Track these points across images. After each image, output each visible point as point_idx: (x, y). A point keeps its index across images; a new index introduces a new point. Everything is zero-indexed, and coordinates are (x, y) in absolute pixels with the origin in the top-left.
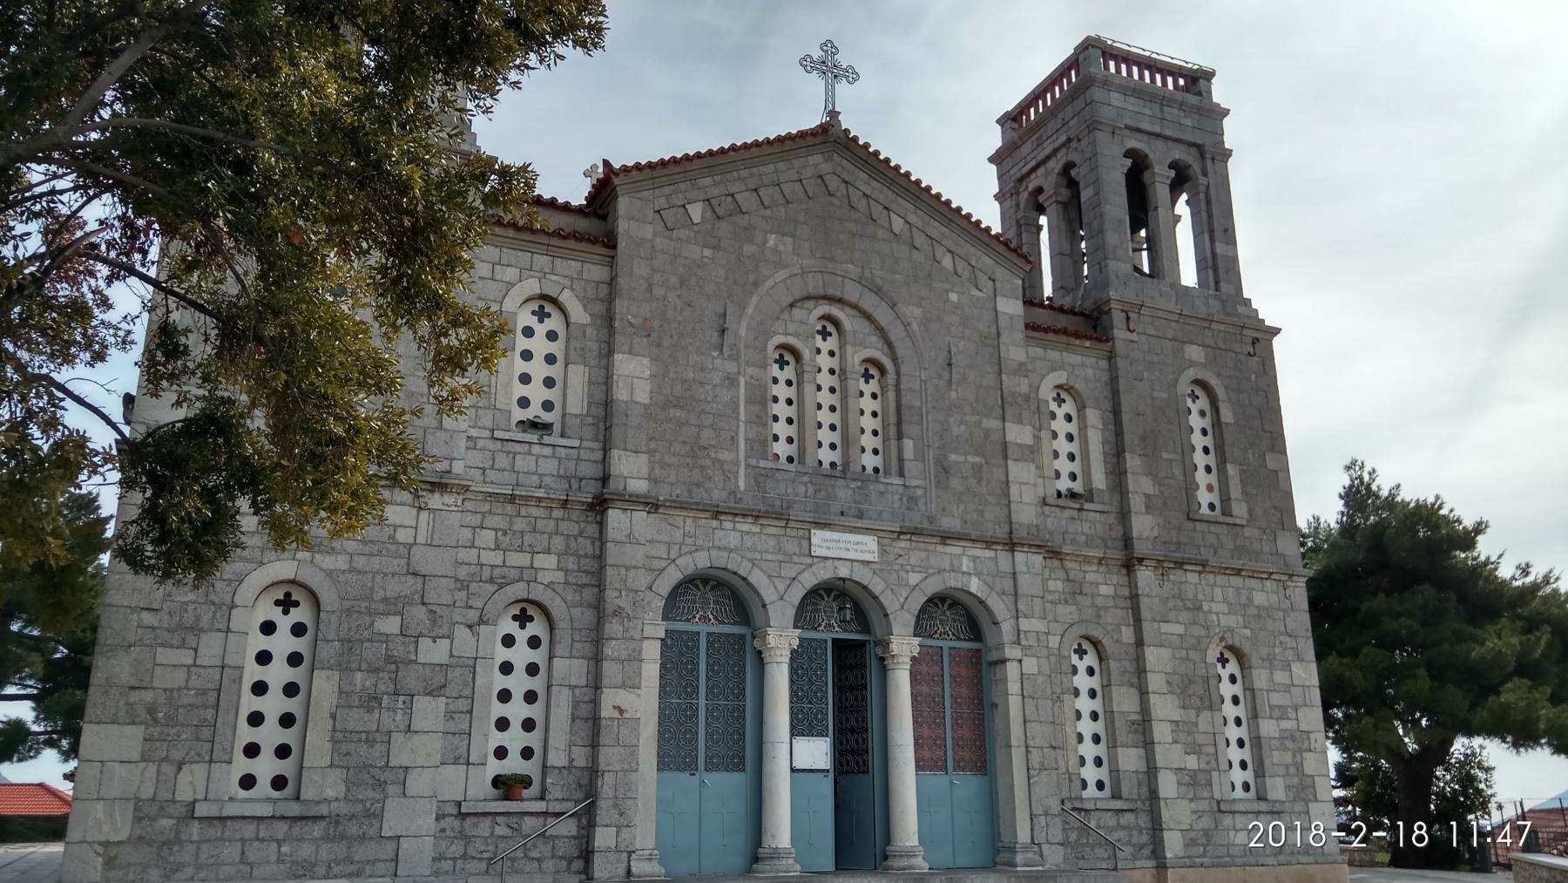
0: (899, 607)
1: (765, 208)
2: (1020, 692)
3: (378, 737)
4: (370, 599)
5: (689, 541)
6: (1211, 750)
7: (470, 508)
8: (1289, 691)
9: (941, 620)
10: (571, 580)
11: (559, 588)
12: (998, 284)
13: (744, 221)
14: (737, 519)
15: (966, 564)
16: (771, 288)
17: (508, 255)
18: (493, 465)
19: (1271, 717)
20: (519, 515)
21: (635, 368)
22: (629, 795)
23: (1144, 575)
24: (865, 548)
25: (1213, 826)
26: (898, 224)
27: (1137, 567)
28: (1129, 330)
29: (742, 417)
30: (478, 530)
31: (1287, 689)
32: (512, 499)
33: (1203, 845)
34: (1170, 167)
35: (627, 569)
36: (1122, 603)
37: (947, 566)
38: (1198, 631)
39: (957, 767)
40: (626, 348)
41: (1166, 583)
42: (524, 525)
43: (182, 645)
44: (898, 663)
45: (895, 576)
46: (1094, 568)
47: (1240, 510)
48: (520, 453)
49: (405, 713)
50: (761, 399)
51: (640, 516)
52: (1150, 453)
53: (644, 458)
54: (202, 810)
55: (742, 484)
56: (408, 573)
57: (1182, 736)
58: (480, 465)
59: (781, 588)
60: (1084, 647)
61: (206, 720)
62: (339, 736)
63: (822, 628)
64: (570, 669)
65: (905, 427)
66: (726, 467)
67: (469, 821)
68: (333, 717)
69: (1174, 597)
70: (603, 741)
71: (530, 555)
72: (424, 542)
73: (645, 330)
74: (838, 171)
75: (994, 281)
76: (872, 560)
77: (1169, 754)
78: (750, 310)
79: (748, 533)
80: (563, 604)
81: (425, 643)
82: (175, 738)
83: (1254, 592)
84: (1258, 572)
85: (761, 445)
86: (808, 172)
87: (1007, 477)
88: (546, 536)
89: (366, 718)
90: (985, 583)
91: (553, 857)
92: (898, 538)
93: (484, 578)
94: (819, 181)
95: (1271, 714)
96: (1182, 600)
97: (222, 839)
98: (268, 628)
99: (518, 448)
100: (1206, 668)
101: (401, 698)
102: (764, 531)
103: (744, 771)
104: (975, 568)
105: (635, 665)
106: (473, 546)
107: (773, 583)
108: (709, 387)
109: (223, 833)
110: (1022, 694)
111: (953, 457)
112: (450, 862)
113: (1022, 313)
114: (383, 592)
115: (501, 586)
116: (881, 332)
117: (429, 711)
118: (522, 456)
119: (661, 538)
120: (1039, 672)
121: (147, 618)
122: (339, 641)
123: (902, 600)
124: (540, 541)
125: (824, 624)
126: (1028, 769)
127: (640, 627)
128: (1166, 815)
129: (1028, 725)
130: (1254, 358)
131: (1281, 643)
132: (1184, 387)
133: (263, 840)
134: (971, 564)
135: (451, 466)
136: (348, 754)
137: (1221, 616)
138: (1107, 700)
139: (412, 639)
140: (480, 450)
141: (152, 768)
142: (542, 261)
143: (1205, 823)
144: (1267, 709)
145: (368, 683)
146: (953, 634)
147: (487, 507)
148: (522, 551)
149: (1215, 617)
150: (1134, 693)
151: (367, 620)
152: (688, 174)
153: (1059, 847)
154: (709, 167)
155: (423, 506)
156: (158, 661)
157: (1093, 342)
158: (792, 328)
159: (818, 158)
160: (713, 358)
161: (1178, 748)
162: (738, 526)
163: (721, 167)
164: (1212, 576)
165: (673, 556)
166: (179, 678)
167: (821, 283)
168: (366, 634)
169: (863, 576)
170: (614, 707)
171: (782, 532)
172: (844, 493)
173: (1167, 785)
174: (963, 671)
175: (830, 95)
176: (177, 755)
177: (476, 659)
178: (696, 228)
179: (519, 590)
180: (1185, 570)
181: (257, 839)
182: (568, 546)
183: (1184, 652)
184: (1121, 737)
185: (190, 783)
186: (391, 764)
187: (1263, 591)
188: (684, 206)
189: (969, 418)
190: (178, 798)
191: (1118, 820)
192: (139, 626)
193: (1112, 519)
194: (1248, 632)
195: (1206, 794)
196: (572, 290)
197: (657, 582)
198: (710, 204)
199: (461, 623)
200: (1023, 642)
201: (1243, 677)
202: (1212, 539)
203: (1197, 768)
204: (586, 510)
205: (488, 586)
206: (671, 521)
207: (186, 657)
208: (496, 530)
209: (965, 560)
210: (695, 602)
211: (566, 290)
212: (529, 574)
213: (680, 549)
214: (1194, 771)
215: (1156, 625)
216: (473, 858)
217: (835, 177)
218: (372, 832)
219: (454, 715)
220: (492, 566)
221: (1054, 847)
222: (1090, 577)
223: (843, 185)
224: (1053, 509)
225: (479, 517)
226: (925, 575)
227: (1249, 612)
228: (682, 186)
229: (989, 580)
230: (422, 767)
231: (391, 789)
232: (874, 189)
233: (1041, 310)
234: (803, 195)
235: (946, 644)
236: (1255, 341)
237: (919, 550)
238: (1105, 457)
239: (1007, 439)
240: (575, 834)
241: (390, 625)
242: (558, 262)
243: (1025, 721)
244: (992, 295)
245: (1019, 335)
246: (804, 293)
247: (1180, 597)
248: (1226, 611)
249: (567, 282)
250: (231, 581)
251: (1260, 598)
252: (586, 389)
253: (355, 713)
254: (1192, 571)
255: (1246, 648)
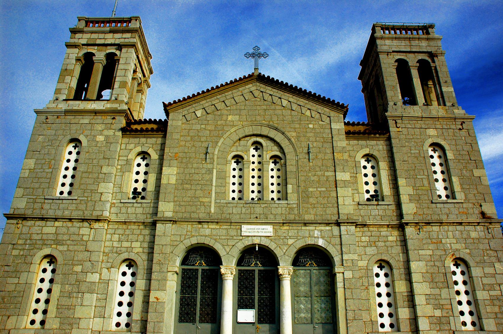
0: (283, 254)
1: (227, 107)
2: (343, 287)
4: (73, 260)
7: (111, 227)
8: (495, 277)
11: (140, 254)
14: (209, 224)
15: (316, 233)
17: (132, 140)
18: (120, 212)
19: (484, 290)
20: (128, 229)
21: (170, 171)
22: (159, 331)
24: (267, 231)
26: (285, 103)
29: (214, 184)
30: (113, 235)
32: (125, 223)
35: (163, 245)
37: (307, 235)
38: (439, 253)
40: (168, 165)
41: (421, 232)
42: (129, 232)
44: (283, 278)
46: (385, 229)
47: (460, 196)
48: (129, 207)
49: (81, 299)
50: (223, 177)
51: (169, 225)
52: (412, 177)
53: (172, 204)
55: (213, 210)
56: (86, 251)
57: (432, 301)
58: (116, 212)
59: (228, 250)
61: (19, 301)
62: (59, 306)
64: (141, 284)
65: (288, 180)
66: (206, 204)
68: (58, 300)
69: (426, 238)
70: (150, 310)
71: (130, 243)
72: (92, 240)
73: (176, 157)
74: (259, 88)
75: (330, 117)
76: (270, 235)
78: (219, 144)
79: (214, 229)
80: (141, 260)
82: (9, 307)
83: (470, 232)
84: (471, 223)
85: (221, 194)
86: (246, 91)
87: (337, 195)
88: (137, 235)
89: (68, 301)
90: (326, 240)
93: (114, 252)
94: (251, 93)
95: (484, 288)
96: (431, 239)
99: (129, 205)
101: (80, 294)
102: (221, 228)
104: (321, 235)
105: (164, 282)
106: (111, 240)
107: (224, 248)
110: (344, 287)
111: (311, 189)
114: (77, 257)
115: (119, 254)
117: (91, 299)
118: (130, 208)
119: (178, 233)
120: (353, 276)
121: (7, 268)
122: (62, 274)
123: (284, 251)
124: (135, 237)
126: (347, 320)
127: (166, 268)
129: (347, 300)
131: (487, 254)
135: (102, 213)
136: (61, 313)
137: (452, 245)
139: (85, 273)
140: (116, 207)
144: (481, 286)
145: (70, 289)
147: (117, 226)
148: (128, 241)
149: (449, 245)
152: (195, 101)
154: (204, 97)
155: (92, 227)
156: (7, 282)
158: (240, 148)
160: (203, 164)
161: (430, 307)
162: (210, 226)
163: (209, 96)
164: (446, 227)
167: (251, 130)
168: (71, 272)
169: (265, 242)
170: (155, 298)
171: (229, 227)
172: (258, 209)
176: (8, 313)
177: (109, 280)
178: (199, 119)
179: (125, 256)
180: (431, 226)
182: (144, 238)
183: (433, 262)
184: (399, 304)
186: (75, 317)
187: (475, 231)
188: (194, 112)
189: (319, 173)
192: (4, 271)
194: (468, 251)
195: (446, 328)
196: (153, 148)
197: (175, 250)
198: (205, 110)
199: (105, 268)
203: (441, 316)
204: (152, 225)
205: (115, 254)
207: (16, 281)
208: (119, 234)
209: (316, 232)
211: (150, 148)
212: (130, 249)
213: (185, 237)
214: (440, 317)
215: (416, 252)
217: (257, 91)
219: (100, 300)
220: (117, 247)
222: (383, 234)
223: (261, 93)
225: (114, 230)
228: (194, 105)
230: (85, 318)
231: (74, 326)
232: (274, 92)
234: (244, 100)
238: (389, 181)
242: (149, 139)
243: (345, 299)
244: (329, 122)
246: (244, 135)
248: (455, 242)
249: (151, 146)
250: (32, 255)
251: (473, 235)
253: (65, 299)
255: (467, 258)
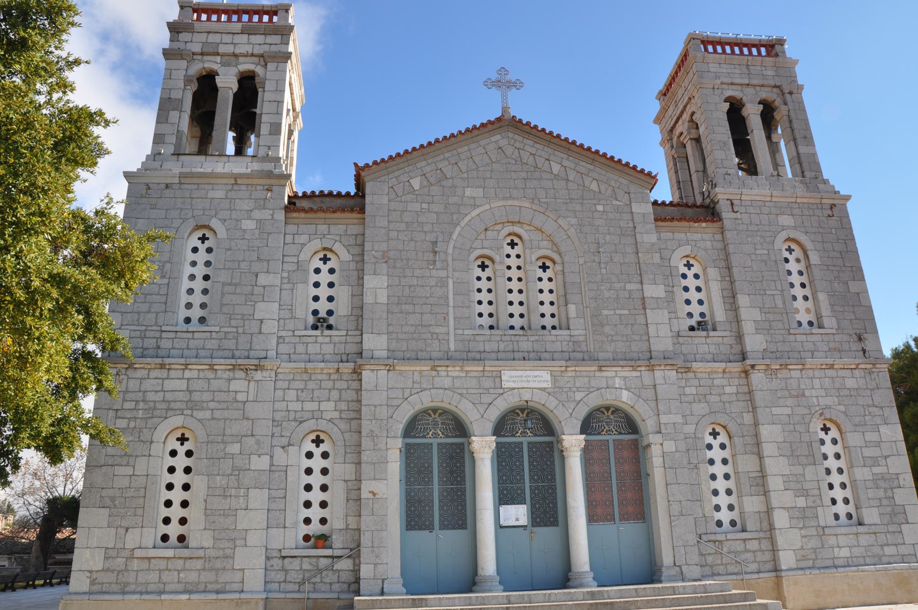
3: (230, 512)
5: (416, 386)
6: (816, 492)
9: (606, 422)
10: (343, 416)
11: (336, 422)
12: (632, 195)
13: (449, 183)
16: (470, 220)
17: (303, 228)
20: (311, 380)
23: (757, 378)
24: (541, 379)
25: (820, 546)
26: (556, 168)
27: (751, 371)
28: (733, 211)
31: (878, 444)
33: (813, 559)
34: (759, 103)
36: (741, 397)
39: (623, 518)
43: (128, 465)
45: (565, 395)
53: (385, 337)
54: (138, 553)
57: (792, 485)
60: (717, 431)
63: (519, 434)
67: (287, 560)
68: (205, 501)
77: (780, 497)
79: (457, 377)
81: (254, 458)
88: (327, 391)
91: (338, 582)
92: (566, 370)
93: (290, 419)
94: (500, 151)
97: (149, 570)
98: (173, 453)
99: (309, 340)
100: (810, 436)
102: (469, 375)
103: (466, 529)
106: (284, 400)
108: (428, 288)
109: (132, 584)
112: (277, 584)
113: (652, 211)
115: (301, 422)
116: (550, 238)
117: (258, 498)
123: (571, 411)
125: (520, 432)
128: (781, 541)
130: (833, 218)
132: (781, 246)
133: (170, 570)
134: (622, 382)
137: (820, 398)
138: (735, 464)
141: (113, 531)
142: (323, 228)
143: (814, 543)
144: (861, 460)
145: (223, 482)
146: (616, 430)
150: (755, 458)
151: (222, 446)
153: (696, 567)
157: (708, 223)
158: (486, 244)
159: (498, 137)
160: (430, 269)
161: (790, 493)
165: (406, 395)
166: (125, 482)
173: (781, 519)
174: (626, 454)
175: (504, 98)
179: (311, 424)
181: (167, 569)
182: (340, 396)
183: (792, 426)
185: (132, 539)
187: (853, 377)
189: (617, 286)
190: (126, 547)
191: (745, 546)
193: (731, 341)
194: (842, 408)
195: (813, 523)
200: (663, 431)
201: (842, 439)
202: (809, 346)
205: (293, 423)
206: (404, 374)
207: (129, 471)
209: (617, 380)
210: (429, 424)
212: (316, 415)
215: (768, 410)
216: (290, 582)
218: (228, 566)
221: (691, 568)
223: (516, 150)
224: (686, 338)
225: (287, 383)
226: (587, 393)
227: (842, 394)
228: (407, 170)
229: (636, 391)
231: (238, 542)
232: (538, 149)
233: (672, 208)
235: (611, 438)
236: (832, 206)
237: (582, 377)
239: (645, 296)
240: (352, 568)
241: (235, 448)
242: (332, 227)
245: (652, 226)
247: (787, 389)
249: (338, 238)
252: (350, 299)
254: (795, 369)
